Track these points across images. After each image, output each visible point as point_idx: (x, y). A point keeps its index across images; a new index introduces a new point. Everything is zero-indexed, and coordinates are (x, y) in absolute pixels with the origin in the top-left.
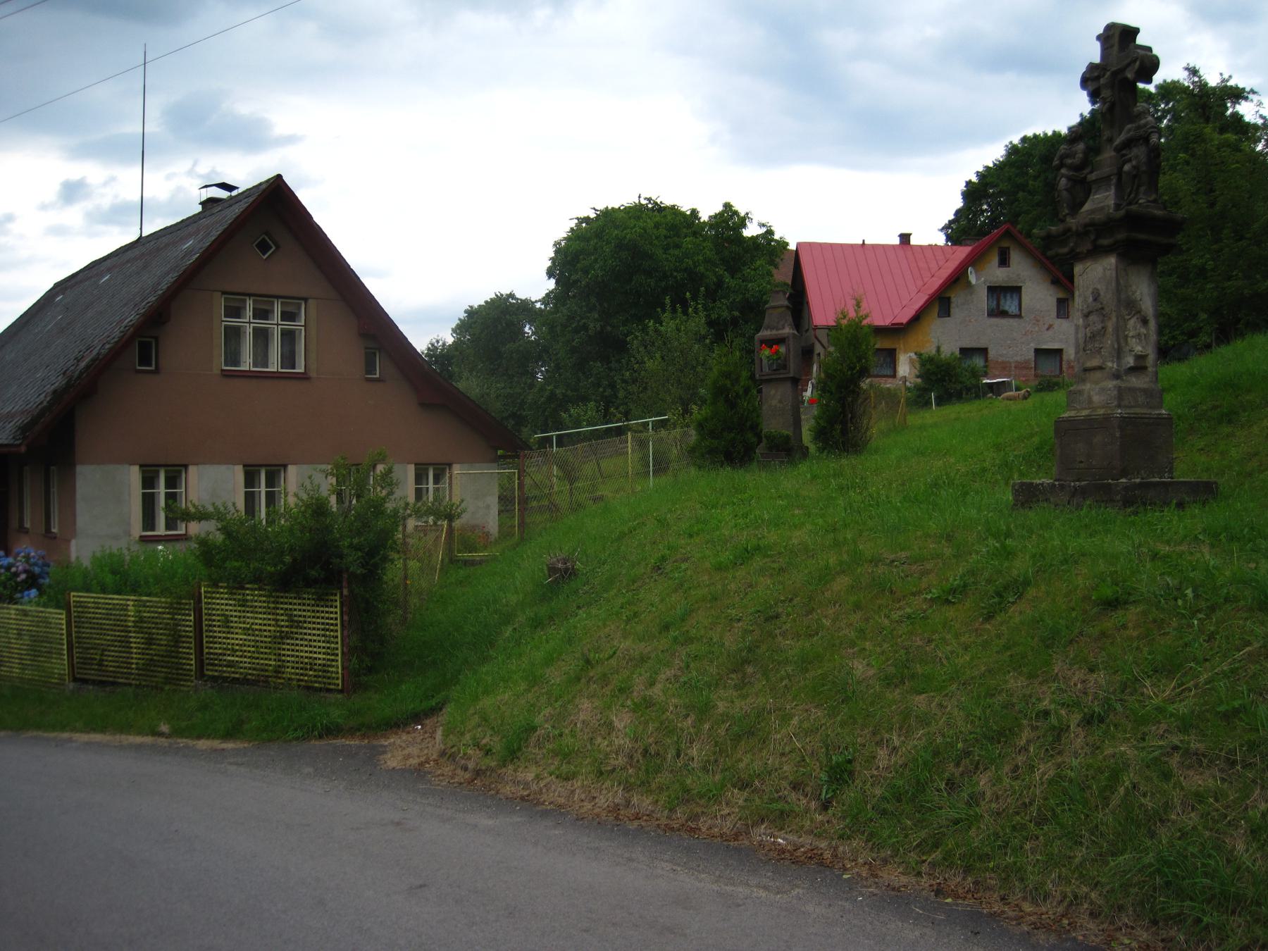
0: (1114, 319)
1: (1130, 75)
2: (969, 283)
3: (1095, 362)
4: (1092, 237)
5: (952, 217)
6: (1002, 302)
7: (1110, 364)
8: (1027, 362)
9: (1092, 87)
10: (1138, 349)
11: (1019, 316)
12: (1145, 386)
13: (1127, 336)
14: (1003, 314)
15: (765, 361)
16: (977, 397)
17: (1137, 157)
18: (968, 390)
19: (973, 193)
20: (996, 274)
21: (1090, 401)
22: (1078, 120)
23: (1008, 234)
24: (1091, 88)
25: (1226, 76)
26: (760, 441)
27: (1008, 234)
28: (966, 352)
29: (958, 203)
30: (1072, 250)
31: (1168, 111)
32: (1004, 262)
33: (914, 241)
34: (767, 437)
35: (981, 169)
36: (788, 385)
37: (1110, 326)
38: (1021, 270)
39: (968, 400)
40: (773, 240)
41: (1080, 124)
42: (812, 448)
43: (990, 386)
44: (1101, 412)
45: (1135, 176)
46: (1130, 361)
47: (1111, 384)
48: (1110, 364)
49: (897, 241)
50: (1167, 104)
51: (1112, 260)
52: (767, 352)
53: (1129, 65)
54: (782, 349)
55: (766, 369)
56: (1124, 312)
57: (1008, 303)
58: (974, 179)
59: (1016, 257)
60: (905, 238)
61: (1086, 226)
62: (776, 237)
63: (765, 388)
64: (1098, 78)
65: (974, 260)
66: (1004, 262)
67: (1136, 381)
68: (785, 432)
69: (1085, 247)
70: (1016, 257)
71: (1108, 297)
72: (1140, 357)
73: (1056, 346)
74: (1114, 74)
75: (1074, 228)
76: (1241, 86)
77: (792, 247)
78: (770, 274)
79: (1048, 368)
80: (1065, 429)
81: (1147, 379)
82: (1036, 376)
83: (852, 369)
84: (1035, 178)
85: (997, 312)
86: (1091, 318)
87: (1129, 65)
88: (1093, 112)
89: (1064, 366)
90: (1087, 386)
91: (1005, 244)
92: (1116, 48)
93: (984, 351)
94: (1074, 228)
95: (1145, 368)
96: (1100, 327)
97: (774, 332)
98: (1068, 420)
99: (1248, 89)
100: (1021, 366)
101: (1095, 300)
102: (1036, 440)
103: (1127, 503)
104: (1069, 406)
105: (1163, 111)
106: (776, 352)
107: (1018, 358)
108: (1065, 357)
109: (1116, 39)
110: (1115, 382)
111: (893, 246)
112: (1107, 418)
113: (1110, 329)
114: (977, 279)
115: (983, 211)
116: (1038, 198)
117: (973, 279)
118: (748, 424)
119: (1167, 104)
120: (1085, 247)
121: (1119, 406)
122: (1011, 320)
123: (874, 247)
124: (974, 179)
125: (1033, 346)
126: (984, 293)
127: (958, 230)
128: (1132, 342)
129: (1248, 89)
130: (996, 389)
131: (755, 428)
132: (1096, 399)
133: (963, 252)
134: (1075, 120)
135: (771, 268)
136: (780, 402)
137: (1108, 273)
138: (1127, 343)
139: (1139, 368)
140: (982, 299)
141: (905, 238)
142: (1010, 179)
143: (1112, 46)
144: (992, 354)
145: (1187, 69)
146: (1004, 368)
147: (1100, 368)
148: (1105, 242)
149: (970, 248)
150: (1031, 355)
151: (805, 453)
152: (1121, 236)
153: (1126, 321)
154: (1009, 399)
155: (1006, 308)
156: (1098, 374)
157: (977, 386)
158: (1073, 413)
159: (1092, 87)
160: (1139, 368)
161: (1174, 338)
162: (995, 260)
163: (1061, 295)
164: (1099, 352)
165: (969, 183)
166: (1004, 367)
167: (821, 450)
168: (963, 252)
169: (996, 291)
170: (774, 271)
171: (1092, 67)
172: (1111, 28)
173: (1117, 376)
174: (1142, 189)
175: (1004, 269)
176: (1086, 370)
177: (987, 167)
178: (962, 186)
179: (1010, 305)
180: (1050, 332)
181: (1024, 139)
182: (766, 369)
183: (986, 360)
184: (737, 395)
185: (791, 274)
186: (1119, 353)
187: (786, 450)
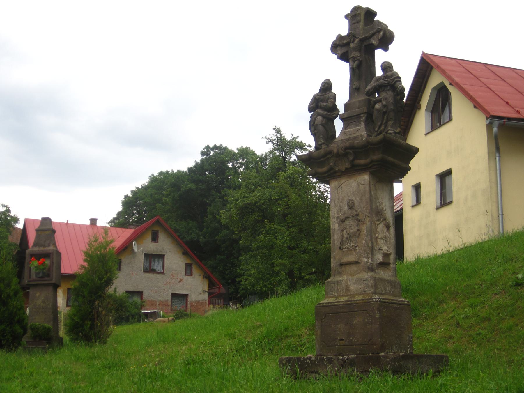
0: (368, 223)
1: (374, 42)
2: (133, 251)
3: (351, 258)
4: (351, 158)
5: (115, 216)
6: (152, 264)
7: (365, 260)
8: (166, 301)
9: (340, 51)
10: (385, 248)
11: (163, 273)
12: (390, 278)
13: (377, 238)
14: (153, 271)
15: (33, 271)
16: (139, 321)
17: (386, 99)
18: (133, 316)
19: (129, 203)
20: (151, 247)
21: (348, 289)
22: (194, 164)
23: (158, 223)
24: (340, 52)
25: (295, 136)
26: (25, 332)
27: (158, 223)
28: (131, 293)
29: (120, 208)
30: (331, 169)
31: (244, 164)
32: (155, 239)
33: (99, 224)
34: (33, 329)
35: (134, 189)
36: (51, 289)
37: (364, 230)
38: (165, 245)
39: (133, 323)
40: (9, 216)
41: (195, 166)
42: (66, 339)
43: (147, 315)
44: (360, 298)
45: (384, 113)
46: (379, 258)
47: (367, 275)
48: (365, 260)
49: (88, 223)
50: (243, 160)
51: (366, 177)
52: (36, 263)
53: (373, 34)
54: (47, 262)
55: (33, 276)
56: (375, 218)
57: (156, 264)
58: (130, 195)
59: (162, 237)
60: (93, 221)
61: (346, 148)
62: (12, 214)
63: (31, 291)
64: (348, 44)
65: (137, 237)
66: (155, 239)
67: (384, 274)
68: (47, 325)
69: (345, 165)
70: (162, 237)
71: (362, 206)
72: (386, 255)
73: (184, 292)
74: (362, 41)
75: (335, 151)
76: (304, 142)
77: (20, 225)
78: (6, 237)
79: (179, 306)
80: (323, 313)
81: (390, 274)
82: (171, 310)
83: (100, 279)
84: (167, 196)
85: (149, 270)
86: (347, 222)
87: (373, 34)
88: (202, 160)
89: (189, 305)
90: (344, 278)
91: (156, 228)
92: (362, 23)
93: (140, 294)
94: (335, 151)
95: (388, 264)
96: (355, 230)
97: (42, 249)
98: (328, 305)
99: (307, 144)
100: (163, 304)
101: (350, 208)
102: (264, 330)
103: (396, 372)
104: (327, 294)
105: (241, 163)
106: (43, 264)
107: (161, 299)
108: (189, 300)
109: (362, 17)
110: (371, 274)
111: (86, 226)
112: (366, 303)
113: (364, 231)
114: (138, 249)
115: (134, 214)
116: (168, 207)
117: (135, 248)
118: (16, 318)
119: (243, 160)
120: (345, 165)
121: (375, 293)
122: (158, 275)
123: (74, 225)
124: (130, 195)
125: (170, 291)
126: (142, 258)
127: (120, 221)
128: (381, 242)
129: (307, 144)
130: (153, 315)
131: (21, 322)
132: (353, 287)
133: (128, 233)
134: (192, 164)
135: (8, 234)
136: (43, 302)
137: (362, 187)
138: (377, 244)
139: (384, 265)
140: (140, 261)
141: (93, 221)
142: (151, 195)
143: (359, 22)
144: (145, 295)
145: (274, 129)
146: (153, 305)
147: (356, 263)
148: (362, 162)
149: (132, 231)
150: (169, 298)
151: (60, 340)
152: (376, 156)
153: (376, 226)
154: (161, 321)
155: (155, 268)
156: (354, 268)
157: (139, 314)
158: (332, 300)
159: (340, 51)
160: (384, 265)
161: (265, 286)
162: (150, 238)
163: (188, 262)
164: (355, 250)
165: (126, 197)
166: (153, 304)
167: (73, 340)
168: (128, 233)
169: (149, 257)
170: (9, 236)
171: (340, 38)
172: (357, 10)
173: (371, 269)
174: (390, 123)
175: (155, 244)
176: (341, 265)
177: (138, 188)
178: (122, 198)
179: (157, 266)
180: (181, 283)
181: (161, 173)
182: (33, 276)
183: (142, 298)
184: (9, 296)
185: (19, 238)
186: (372, 251)
187: (46, 339)
